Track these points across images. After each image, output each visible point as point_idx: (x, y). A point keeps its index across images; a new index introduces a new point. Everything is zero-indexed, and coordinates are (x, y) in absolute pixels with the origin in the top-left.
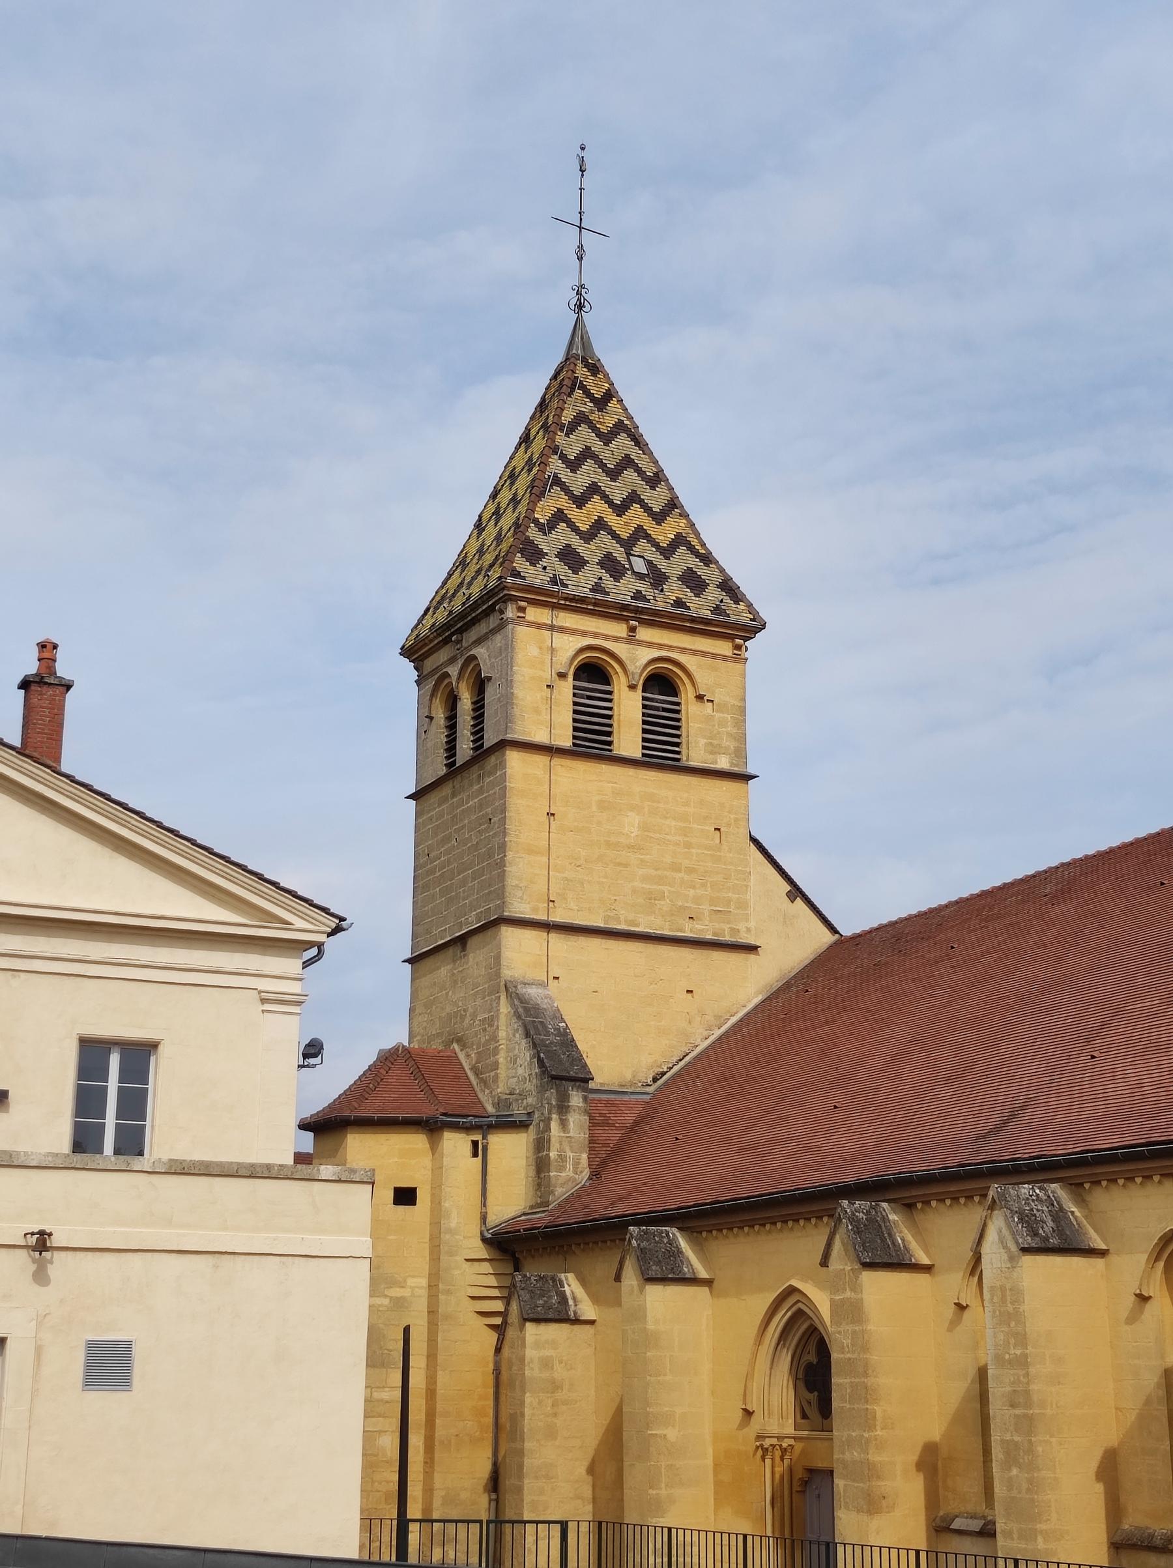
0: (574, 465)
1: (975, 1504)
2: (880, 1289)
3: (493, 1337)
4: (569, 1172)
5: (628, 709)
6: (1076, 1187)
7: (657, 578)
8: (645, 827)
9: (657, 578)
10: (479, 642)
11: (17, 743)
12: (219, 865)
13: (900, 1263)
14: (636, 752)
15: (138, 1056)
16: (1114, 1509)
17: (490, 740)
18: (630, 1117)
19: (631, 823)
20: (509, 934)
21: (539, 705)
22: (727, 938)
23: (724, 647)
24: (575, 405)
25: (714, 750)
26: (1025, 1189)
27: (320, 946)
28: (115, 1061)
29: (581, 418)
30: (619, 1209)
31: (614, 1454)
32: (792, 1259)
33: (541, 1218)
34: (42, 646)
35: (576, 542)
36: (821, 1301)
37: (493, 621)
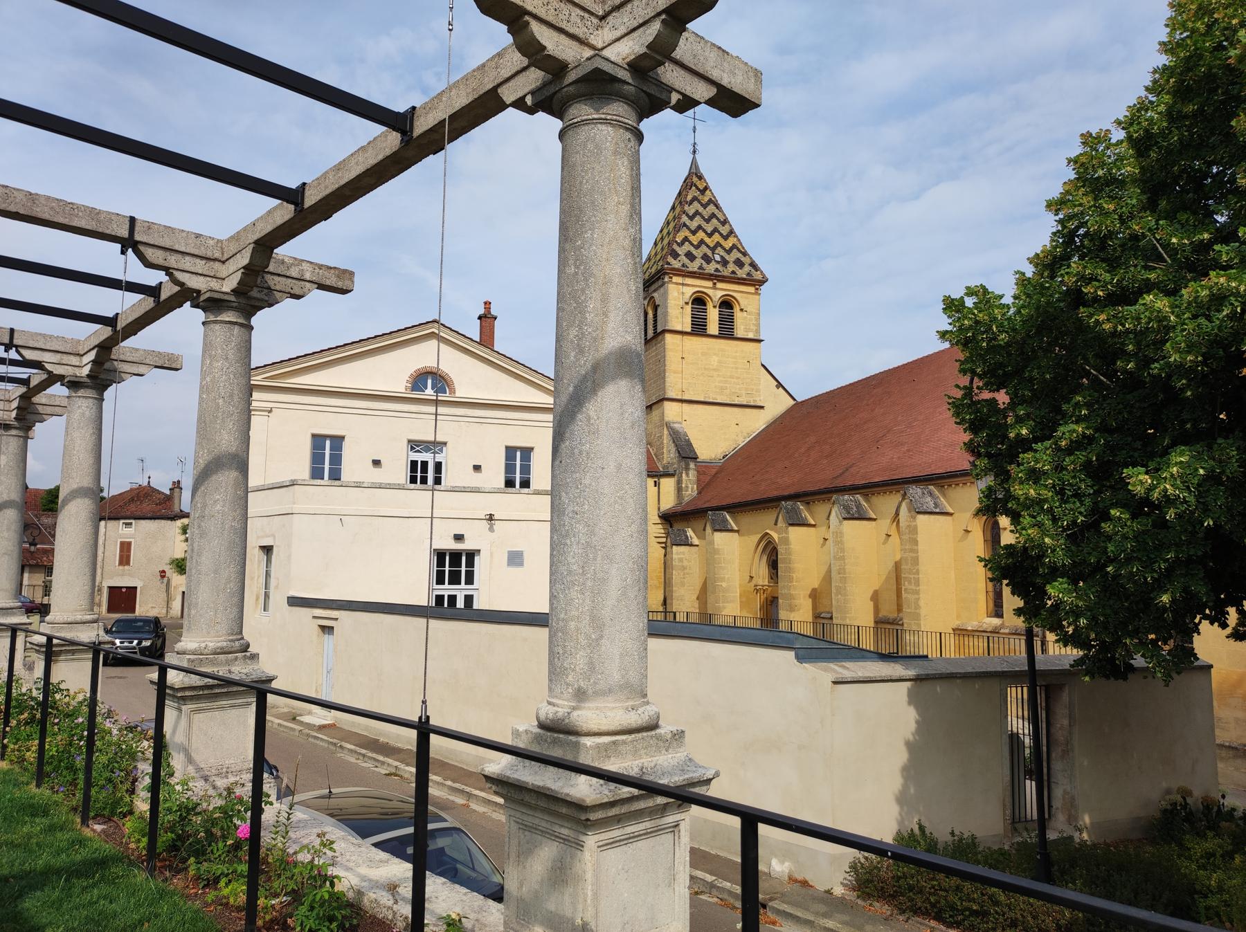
0: (691, 218)
2: (795, 533)
5: (713, 316)
6: (866, 496)
7: (724, 263)
8: (720, 362)
9: (724, 263)
15: (338, 441)
16: (877, 609)
18: (714, 471)
19: (714, 361)
20: (666, 404)
21: (678, 315)
23: (752, 289)
24: (693, 193)
25: (747, 330)
26: (846, 497)
28: (518, 454)
29: (695, 199)
31: (703, 594)
32: (767, 523)
33: (679, 509)
35: (692, 249)
36: (775, 536)
37: (660, 282)
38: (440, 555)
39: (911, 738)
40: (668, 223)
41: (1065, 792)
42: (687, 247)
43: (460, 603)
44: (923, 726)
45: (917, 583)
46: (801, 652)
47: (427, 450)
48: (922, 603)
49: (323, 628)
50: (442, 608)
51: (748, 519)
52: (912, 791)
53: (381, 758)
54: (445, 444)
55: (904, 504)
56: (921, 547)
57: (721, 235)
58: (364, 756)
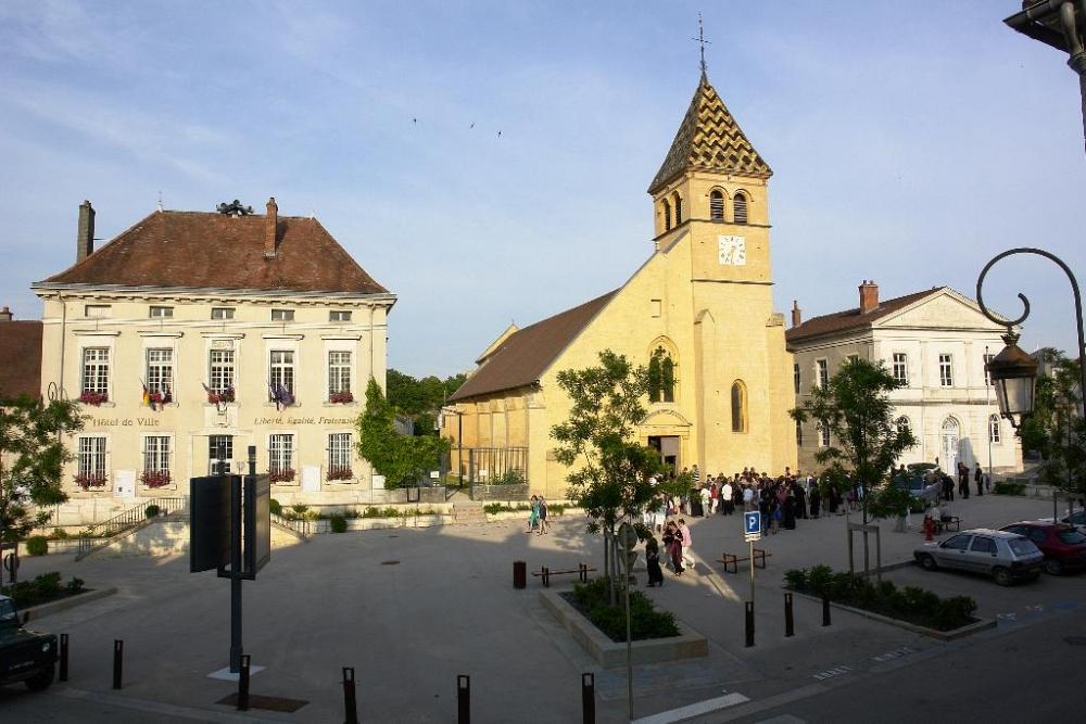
20: (692, 223)
29: (706, 106)
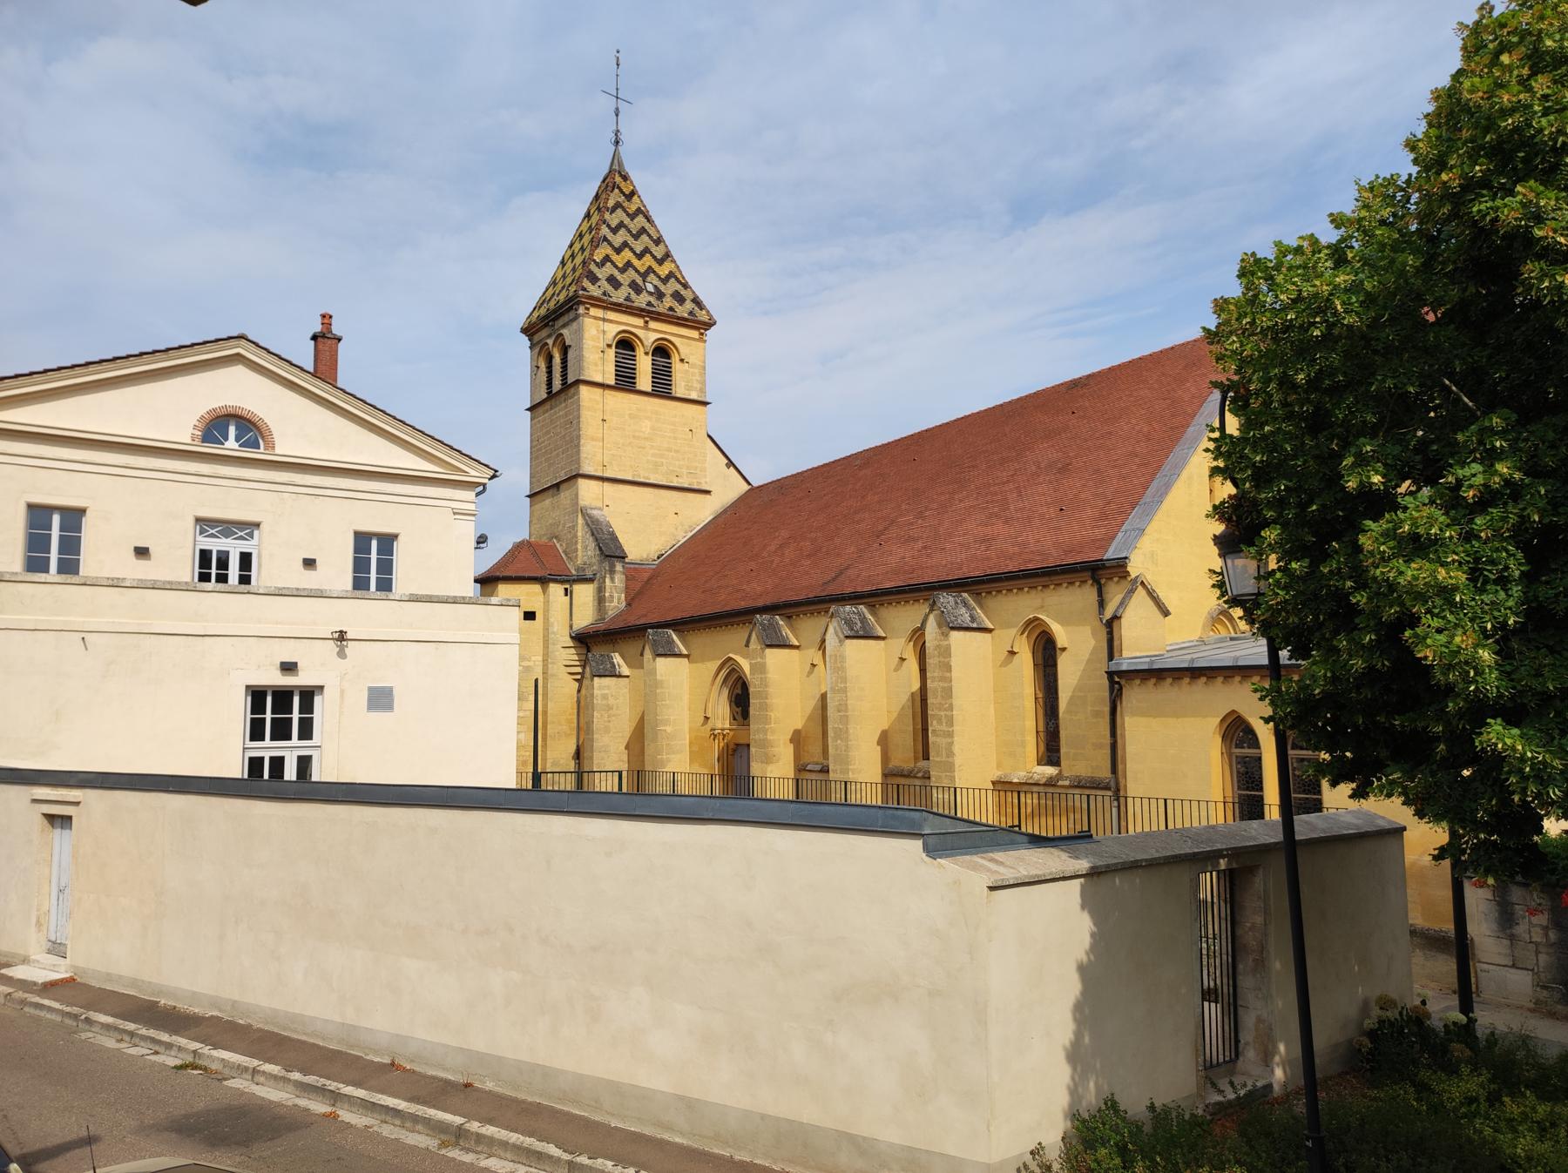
0: (615, 231)
1: (818, 758)
2: (774, 657)
3: (576, 685)
4: (615, 603)
5: (644, 365)
6: (871, 607)
8: (653, 428)
9: (660, 295)
10: (564, 326)
11: (311, 370)
12: (429, 440)
13: (785, 645)
14: (649, 389)
17: (570, 380)
18: (646, 576)
19: (646, 427)
20: (581, 481)
21: (597, 362)
22: (695, 487)
23: (695, 334)
25: (689, 388)
26: (848, 608)
27: (484, 485)
28: (374, 543)
29: (618, 205)
30: (642, 621)
31: (638, 741)
33: (602, 626)
34: (324, 316)
35: (616, 273)
36: (745, 665)
37: (572, 314)
38: (257, 696)
39: (1085, 959)
40: (581, 236)
41: (1259, 1020)
42: (608, 269)
43: (290, 773)
44: (1101, 942)
45: (950, 722)
46: (931, 840)
47: (227, 533)
48: (956, 749)
49: (51, 818)
50: (262, 780)
51: (702, 640)
52: (1087, 1040)
53: (165, 1037)
54: (257, 525)
55: (931, 618)
56: (955, 674)
57: (654, 257)
58: (132, 1034)
